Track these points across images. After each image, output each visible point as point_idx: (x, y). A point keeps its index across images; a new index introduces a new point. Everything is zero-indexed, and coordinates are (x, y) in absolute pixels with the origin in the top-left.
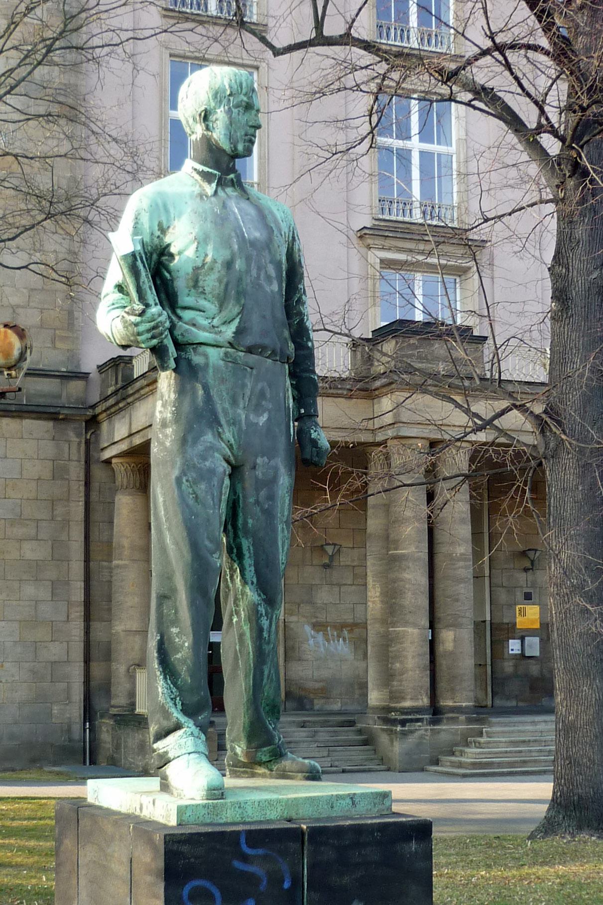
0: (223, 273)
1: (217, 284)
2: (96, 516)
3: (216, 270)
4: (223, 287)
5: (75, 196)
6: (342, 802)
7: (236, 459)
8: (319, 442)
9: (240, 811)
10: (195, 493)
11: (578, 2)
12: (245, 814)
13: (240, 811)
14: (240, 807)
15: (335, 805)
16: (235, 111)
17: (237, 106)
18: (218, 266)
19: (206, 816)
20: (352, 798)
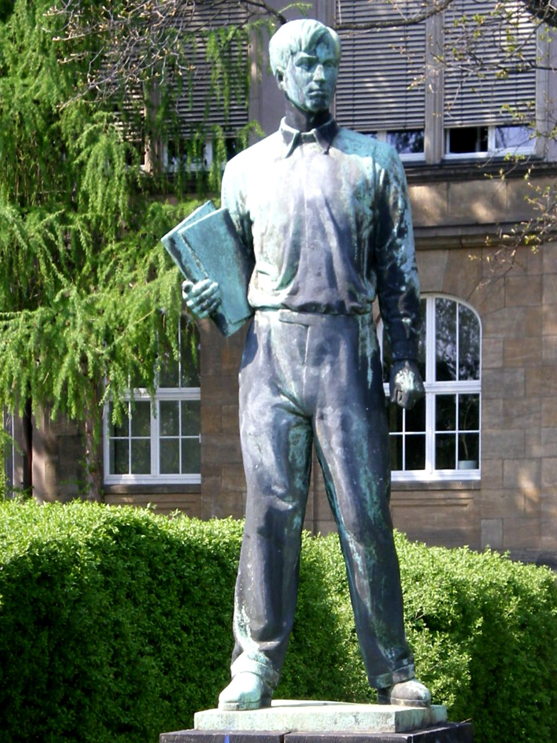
0: (281, 236)
1: (277, 249)
2: (403, 489)
3: (275, 235)
4: (281, 250)
5: (107, 184)
6: (345, 719)
7: (303, 410)
8: (402, 386)
9: (250, 721)
10: (257, 445)
11: (555, 577)
12: (254, 725)
13: (250, 721)
14: (250, 718)
15: (338, 721)
16: (298, 69)
17: (300, 64)
18: (277, 231)
19: (220, 724)
20: (355, 716)
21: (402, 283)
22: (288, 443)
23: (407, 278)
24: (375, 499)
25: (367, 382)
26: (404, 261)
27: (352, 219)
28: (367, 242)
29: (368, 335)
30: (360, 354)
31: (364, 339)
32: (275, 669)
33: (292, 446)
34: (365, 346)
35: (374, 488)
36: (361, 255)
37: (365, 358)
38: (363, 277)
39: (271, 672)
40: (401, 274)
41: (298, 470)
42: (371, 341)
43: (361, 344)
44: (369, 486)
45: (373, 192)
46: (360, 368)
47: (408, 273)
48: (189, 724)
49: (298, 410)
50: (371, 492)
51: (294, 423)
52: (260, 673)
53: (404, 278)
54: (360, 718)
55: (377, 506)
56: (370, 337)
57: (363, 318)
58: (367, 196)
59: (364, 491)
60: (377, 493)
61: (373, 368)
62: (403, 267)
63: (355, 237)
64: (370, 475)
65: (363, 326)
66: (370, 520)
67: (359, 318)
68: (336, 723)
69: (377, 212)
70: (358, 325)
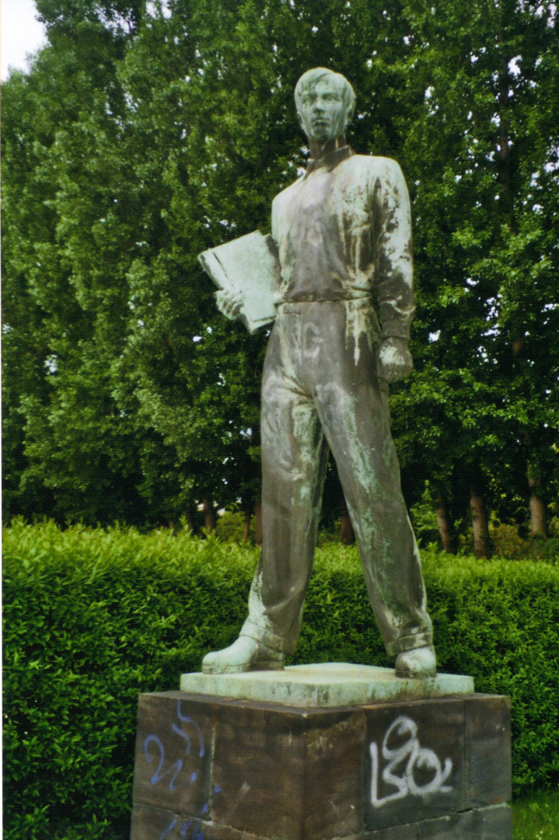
15: (276, 691)
21: (390, 269)
22: (291, 421)
23: (394, 266)
24: (369, 468)
25: (353, 360)
26: (393, 251)
27: (340, 219)
28: (359, 240)
29: (357, 318)
30: (347, 334)
31: (351, 322)
32: (276, 633)
33: (296, 423)
34: (352, 328)
35: (367, 458)
36: (351, 249)
37: (352, 338)
38: (354, 269)
39: (271, 636)
40: (389, 262)
41: (304, 444)
42: (359, 324)
43: (348, 326)
44: (362, 456)
45: (365, 196)
46: (346, 348)
47: (396, 261)
48: (176, 686)
49: (300, 390)
50: (364, 462)
51: (296, 402)
52: (256, 637)
53: (391, 266)
54: (292, 688)
55: (372, 475)
56: (359, 320)
57: (350, 303)
58: (358, 199)
59: (355, 461)
60: (370, 463)
61: (360, 347)
62: (391, 257)
63: (342, 234)
64: (360, 444)
65: (351, 310)
66: (365, 490)
67: (347, 303)
68: (274, 693)
69: (371, 213)
70: (345, 310)
